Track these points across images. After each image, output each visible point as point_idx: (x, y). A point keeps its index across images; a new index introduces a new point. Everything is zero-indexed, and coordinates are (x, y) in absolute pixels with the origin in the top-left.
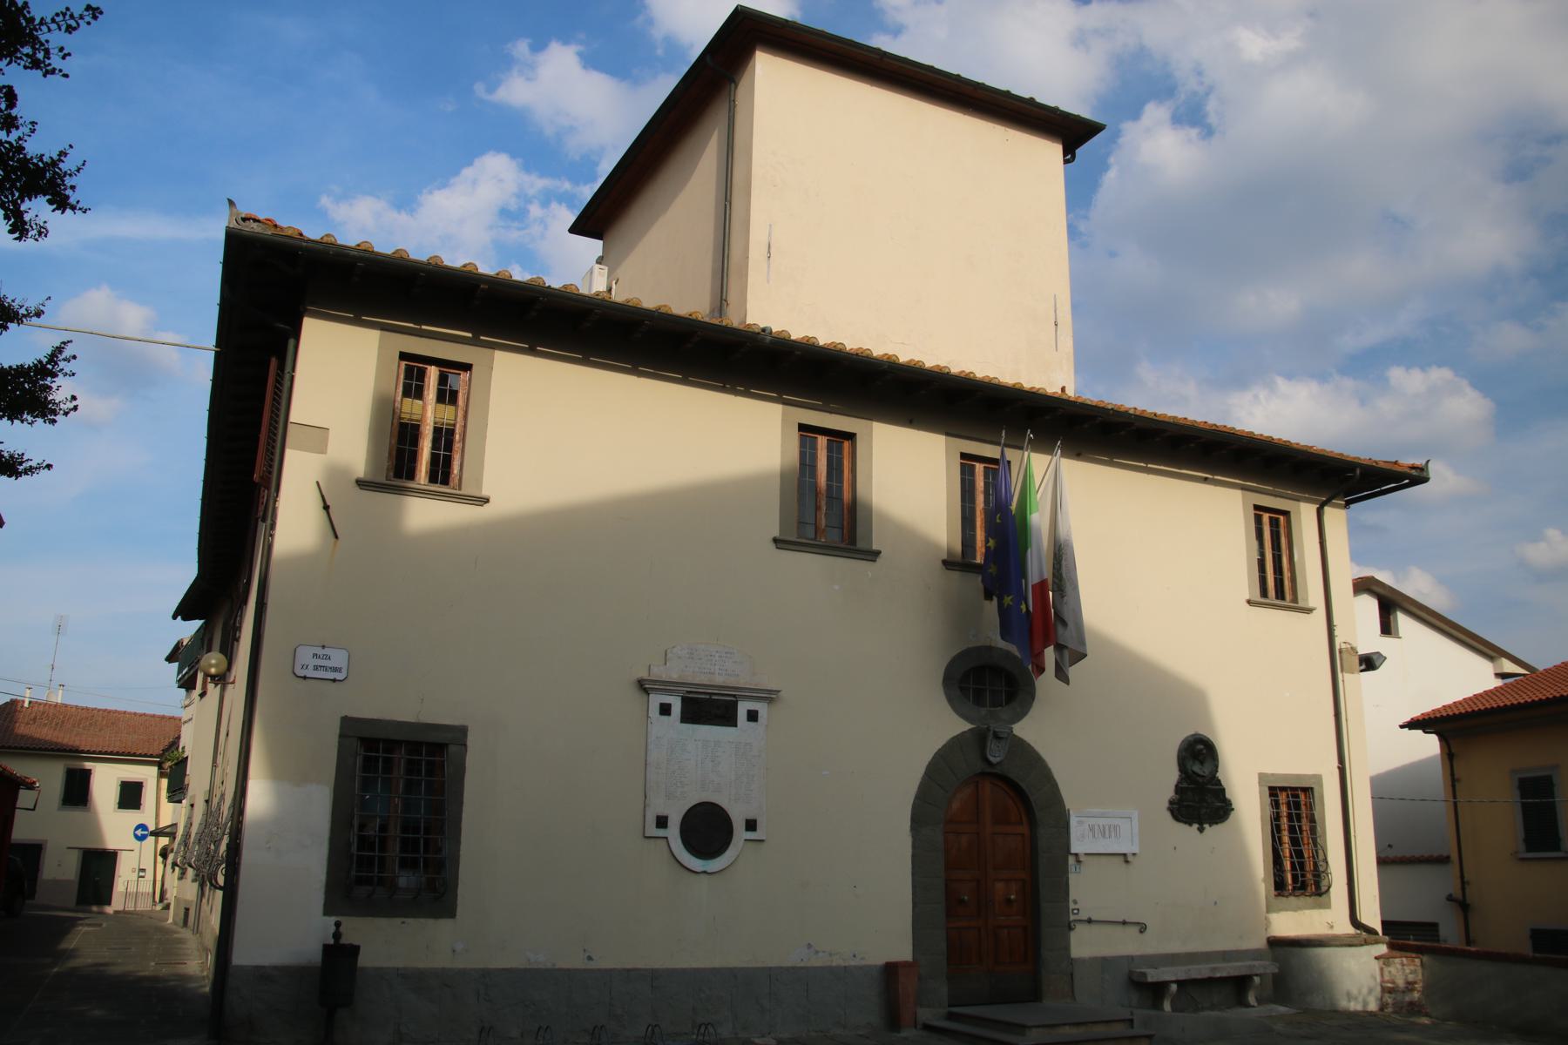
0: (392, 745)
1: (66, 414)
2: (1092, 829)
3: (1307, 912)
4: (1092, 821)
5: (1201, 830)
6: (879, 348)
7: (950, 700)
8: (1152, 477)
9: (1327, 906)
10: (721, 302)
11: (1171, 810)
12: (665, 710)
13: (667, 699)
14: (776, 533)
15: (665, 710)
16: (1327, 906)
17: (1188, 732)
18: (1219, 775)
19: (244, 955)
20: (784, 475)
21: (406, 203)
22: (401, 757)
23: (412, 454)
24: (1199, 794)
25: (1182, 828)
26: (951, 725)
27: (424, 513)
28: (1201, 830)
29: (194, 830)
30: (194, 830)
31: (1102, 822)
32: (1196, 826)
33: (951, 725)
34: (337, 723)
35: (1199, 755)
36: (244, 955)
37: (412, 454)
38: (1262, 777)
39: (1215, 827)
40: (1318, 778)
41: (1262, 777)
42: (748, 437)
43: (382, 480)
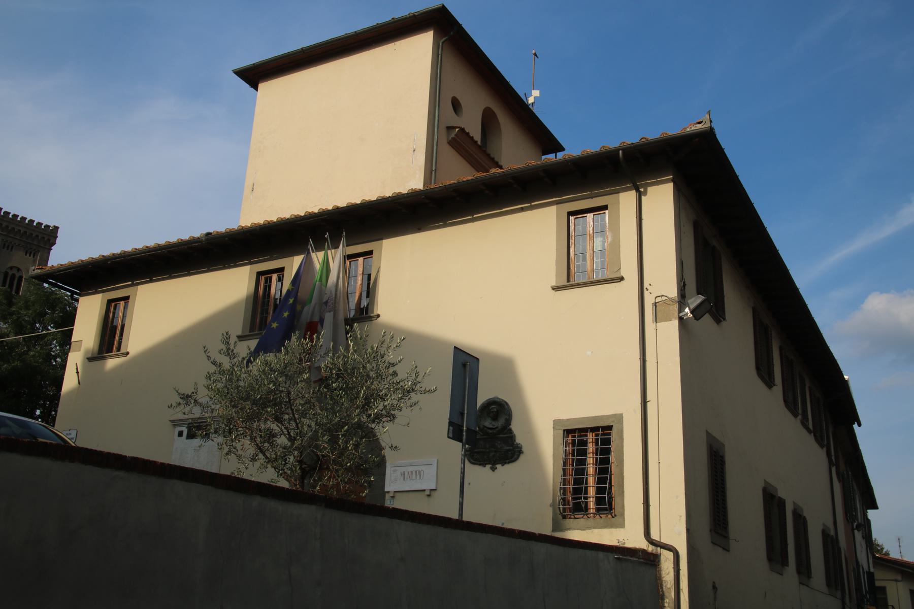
0: (583, 431)
1: (220, 365)
2: (403, 475)
3: (596, 531)
5: (493, 469)
8: (535, 211)
9: (622, 525)
12: (180, 434)
14: (554, 284)
15: (180, 434)
16: (622, 525)
18: (515, 427)
20: (248, 298)
23: (110, 336)
27: (112, 363)
28: (493, 469)
31: (410, 469)
32: (488, 467)
34: (52, 224)
37: (110, 336)
38: (556, 423)
39: (506, 466)
40: (619, 418)
41: (556, 423)
42: (231, 286)
43: (248, 333)
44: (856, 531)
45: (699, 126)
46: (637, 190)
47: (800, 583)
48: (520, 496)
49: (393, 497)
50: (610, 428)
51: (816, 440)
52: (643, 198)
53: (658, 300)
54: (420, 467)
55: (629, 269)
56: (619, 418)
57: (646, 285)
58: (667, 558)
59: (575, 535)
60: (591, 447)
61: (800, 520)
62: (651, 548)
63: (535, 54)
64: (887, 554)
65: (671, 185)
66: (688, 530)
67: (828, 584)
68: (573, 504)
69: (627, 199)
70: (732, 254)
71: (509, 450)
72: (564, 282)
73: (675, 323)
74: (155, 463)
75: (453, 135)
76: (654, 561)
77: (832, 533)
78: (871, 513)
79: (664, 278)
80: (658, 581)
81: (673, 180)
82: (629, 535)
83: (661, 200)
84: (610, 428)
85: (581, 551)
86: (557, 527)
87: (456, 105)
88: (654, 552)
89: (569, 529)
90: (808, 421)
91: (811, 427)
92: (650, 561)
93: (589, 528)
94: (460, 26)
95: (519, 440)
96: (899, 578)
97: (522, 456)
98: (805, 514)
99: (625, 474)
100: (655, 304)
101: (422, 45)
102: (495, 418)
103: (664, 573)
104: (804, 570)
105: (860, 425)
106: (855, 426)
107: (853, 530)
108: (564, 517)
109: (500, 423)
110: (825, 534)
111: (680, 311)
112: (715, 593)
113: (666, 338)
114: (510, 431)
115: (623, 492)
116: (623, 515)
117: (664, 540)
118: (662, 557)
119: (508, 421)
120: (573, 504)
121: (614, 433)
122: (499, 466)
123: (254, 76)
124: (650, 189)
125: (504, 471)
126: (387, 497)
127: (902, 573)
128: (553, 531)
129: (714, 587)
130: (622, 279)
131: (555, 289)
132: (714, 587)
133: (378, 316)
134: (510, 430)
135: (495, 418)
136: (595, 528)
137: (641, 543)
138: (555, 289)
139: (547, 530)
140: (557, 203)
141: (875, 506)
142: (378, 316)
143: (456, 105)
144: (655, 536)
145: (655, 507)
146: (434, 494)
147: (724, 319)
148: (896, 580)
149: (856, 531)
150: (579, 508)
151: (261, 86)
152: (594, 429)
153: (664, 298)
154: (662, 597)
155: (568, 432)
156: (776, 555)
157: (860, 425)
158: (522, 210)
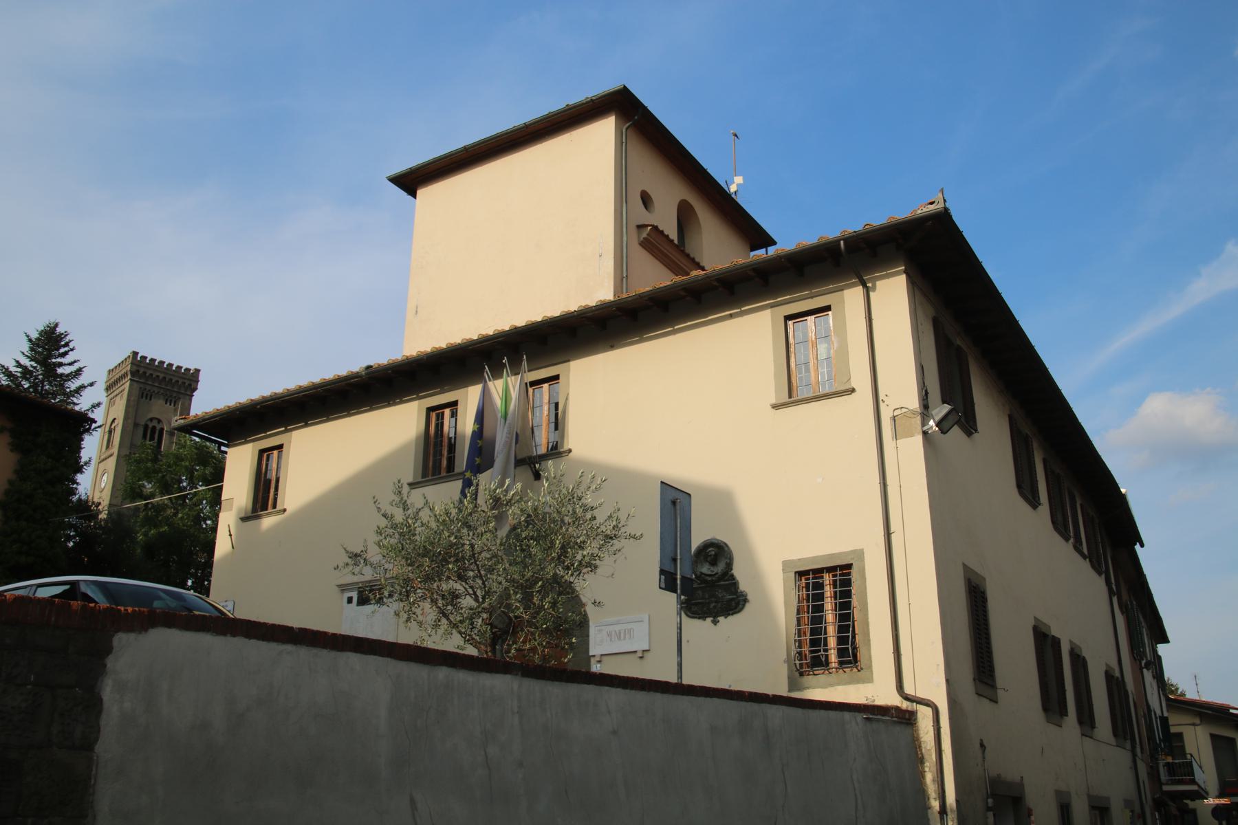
0: (818, 572)
2: (609, 635)
3: (840, 688)
4: (611, 628)
5: (715, 622)
6: (316, 378)
8: (746, 317)
9: (870, 680)
11: (746, 601)
12: (350, 600)
13: (350, 594)
14: (774, 401)
16: (870, 680)
17: (721, 537)
18: (737, 571)
20: (417, 438)
21: (81, 423)
22: (827, 578)
23: (265, 493)
28: (715, 622)
31: (617, 628)
32: (709, 620)
36: (859, 291)
37: (265, 493)
38: (786, 565)
39: (730, 618)
40: (860, 554)
41: (786, 565)
42: (397, 426)
46: (864, 285)
48: (749, 650)
50: (849, 566)
51: (1093, 567)
56: (860, 554)
57: (881, 397)
60: (828, 591)
62: (905, 705)
64: (1183, 694)
66: (947, 681)
67: (1115, 734)
68: (811, 658)
69: (852, 297)
71: (732, 600)
72: (786, 399)
73: (919, 439)
75: (644, 235)
77: (1117, 674)
78: (1162, 649)
80: (915, 743)
81: (905, 272)
83: (893, 294)
84: (849, 566)
86: (793, 685)
87: (646, 199)
91: (1085, 551)
93: (832, 685)
94: (645, 108)
95: (743, 586)
96: (1198, 721)
97: (747, 605)
100: (894, 418)
101: (605, 130)
102: (714, 563)
104: (1087, 720)
105: (1142, 545)
106: (1137, 547)
107: (1141, 669)
108: (801, 674)
109: (720, 568)
110: (1109, 676)
113: (909, 455)
116: (870, 667)
117: (920, 695)
119: (729, 566)
120: (811, 658)
122: (721, 619)
123: (411, 182)
126: (593, 660)
129: (982, 745)
130: (853, 390)
131: (776, 407)
132: (982, 745)
133: (570, 451)
134: (732, 575)
135: (714, 563)
136: (839, 684)
138: (776, 407)
139: (782, 690)
140: (772, 306)
141: (1165, 640)
142: (570, 451)
143: (646, 199)
145: (908, 656)
148: (1194, 724)
150: (818, 662)
151: (420, 192)
152: (830, 570)
154: (922, 761)
155: (800, 574)
157: (1142, 545)
158: (731, 316)
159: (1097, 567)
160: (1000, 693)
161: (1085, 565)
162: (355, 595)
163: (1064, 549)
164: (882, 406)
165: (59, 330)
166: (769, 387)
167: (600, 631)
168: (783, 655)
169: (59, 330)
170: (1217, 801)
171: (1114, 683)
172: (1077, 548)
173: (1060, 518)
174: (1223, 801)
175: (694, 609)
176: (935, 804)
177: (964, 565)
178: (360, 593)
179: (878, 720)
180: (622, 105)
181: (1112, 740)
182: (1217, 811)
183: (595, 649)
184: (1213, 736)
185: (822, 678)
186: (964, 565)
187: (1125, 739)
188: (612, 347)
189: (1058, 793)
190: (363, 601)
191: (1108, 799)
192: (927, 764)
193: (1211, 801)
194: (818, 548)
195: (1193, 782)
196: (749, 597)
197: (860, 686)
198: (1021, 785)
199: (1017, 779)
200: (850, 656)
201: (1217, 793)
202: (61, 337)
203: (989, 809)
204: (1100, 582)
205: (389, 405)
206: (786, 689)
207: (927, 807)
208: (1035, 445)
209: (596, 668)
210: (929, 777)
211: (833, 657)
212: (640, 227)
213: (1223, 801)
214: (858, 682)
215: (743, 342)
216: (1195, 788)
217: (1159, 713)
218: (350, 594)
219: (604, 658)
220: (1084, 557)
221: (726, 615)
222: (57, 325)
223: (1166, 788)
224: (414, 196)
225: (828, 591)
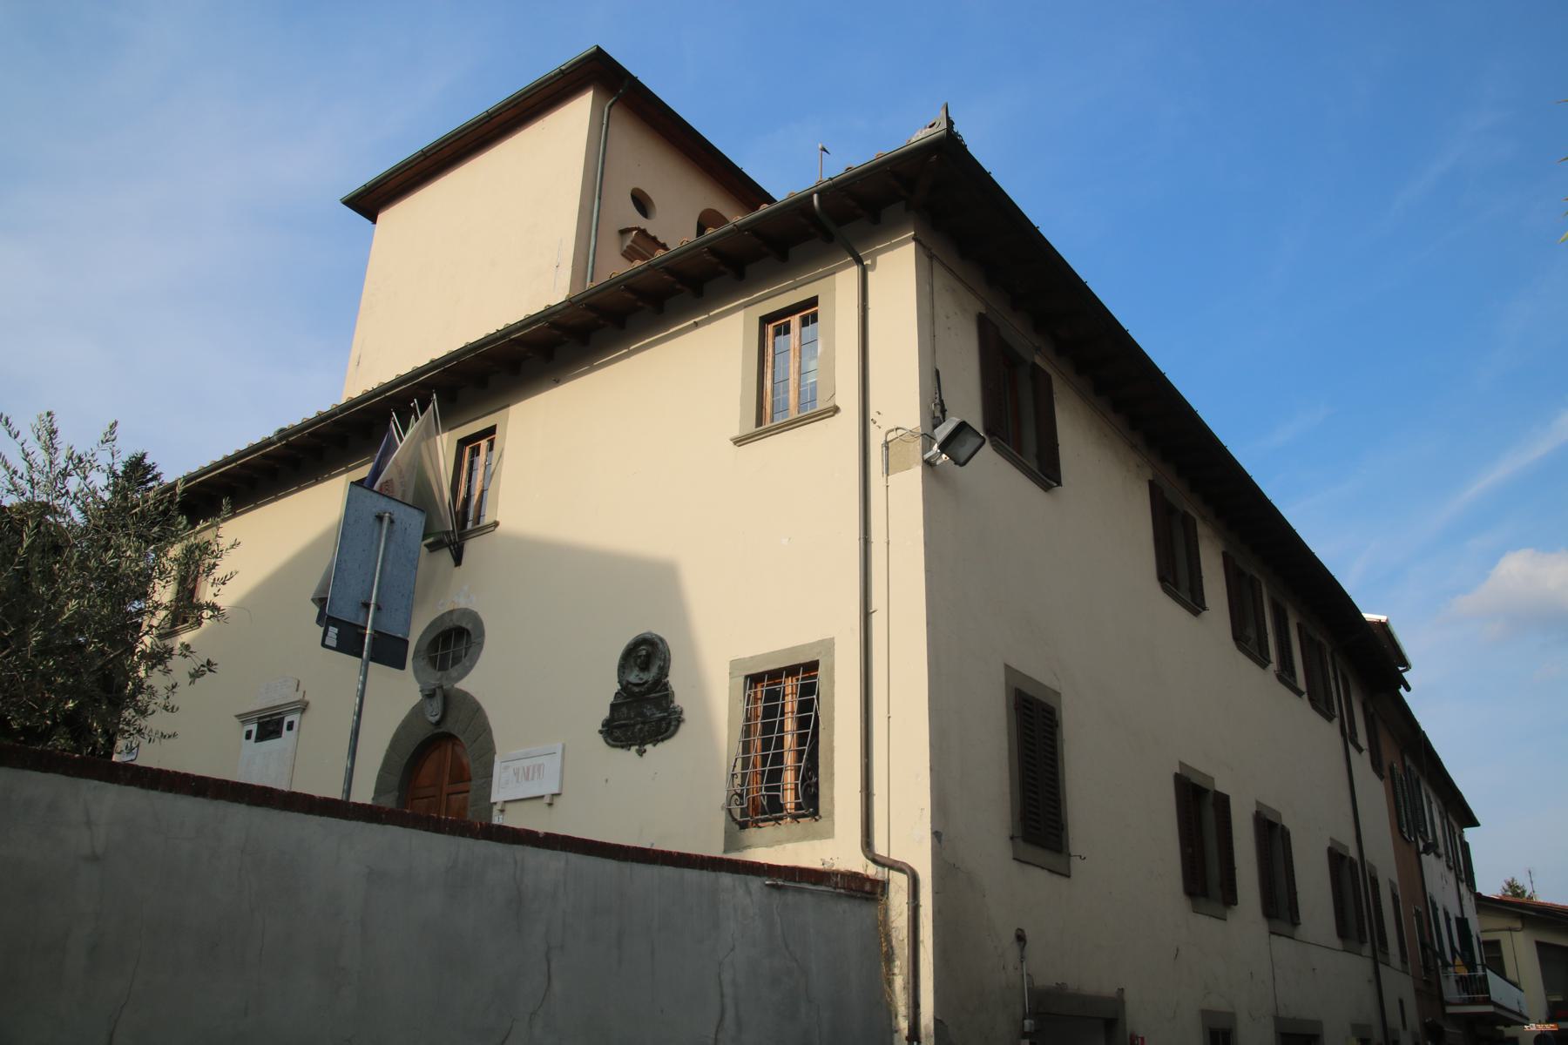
0: (775, 675)
2: (516, 774)
3: (789, 846)
4: (517, 764)
5: (641, 753)
7: (480, 645)
9: (829, 834)
10: (348, 791)
13: (248, 727)
14: (736, 433)
16: (829, 834)
18: (675, 680)
19: (854, 271)
24: (643, 706)
25: (619, 753)
26: (472, 683)
28: (641, 753)
29: (1457, 945)
30: (1457, 945)
31: (526, 763)
32: (634, 748)
33: (472, 683)
35: (646, 657)
36: (854, 271)
38: (734, 664)
39: (660, 745)
40: (828, 645)
41: (734, 664)
44: (1424, 856)
45: (934, 129)
46: (859, 261)
47: (1272, 933)
48: (678, 795)
49: (502, 811)
50: (812, 666)
51: (1315, 707)
52: (870, 274)
53: (891, 436)
54: (549, 763)
55: (847, 398)
56: (828, 645)
57: (872, 414)
58: (899, 882)
59: (761, 854)
60: (785, 699)
61: (1270, 832)
62: (872, 871)
63: (824, 150)
64: (1530, 898)
65: (912, 245)
66: (936, 835)
67: (1342, 932)
68: (757, 806)
69: (846, 280)
70: (1047, 362)
71: (663, 718)
72: (751, 427)
73: (917, 471)
74: (311, 797)
75: (628, 242)
76: (873, 893)
77: (1353, 853)
78: (1469, 834)
79: (900, 402)
80: (882, 929)
81: (915, 239)
82: (835, 849)
83: (897, 269)
84: (812, 666)
85: (669, 871)
86: (731, 842)
87: (642, 203)
88: (879, 877)
89: (749, 847)
90: (1293, 674)
91: (1301, 683)
92: (864, 891)
93: (780, 842)
94: (634, 80)
95: (680, 700)
96: (1518, 925)
97: (683, 727)
98: (1287, 821)
99: (836, 744)
100: (886, 445)
101: (578, 113)
102: (645, 667)
103: (893, 914)
104: (1280, 906)
105: (1408, 689)
106: (1402, 690)
107: (1418, 854)
108: (743, 826)
109: (650, 676)
110: (1336, 858)
111: (924, 452)
112: (1022, 949)
113: (903, 495)
114: (666, 686)
115: (832, 774)
116: (831, 814)
117: (896, 856)
118: (892, 886)
119: (664, 671)
120: (757, 806)
121: (821, 672)
122: (649, 747)
123: (370, 201)
124: (880, 259)
125: (656, 752)
126: (496, 809)
127: (1522, 917)
128: (725, 851)
129: (1021, 938)
130: (836, 410)
131: (739, 441)
132: (1021, 938)
133: (496, 524)
134: (666, 684)
135: (645, 667)
136: (788, 841)
137: (856, 863)
138: (739, 441)
139: (716, 850)
140: (746, 305)
141: (1474, 823)
142: (496, 524)
143: (642, 203)
144: (880, 849)
145: (888, 802)
146: (557, 800)
147: (1059, 484)
148: (1510, 930)
149: (1424, 856)
150: (773, 810)
151: (381, 217)
152: (792, 671)
153: (900, 432)
154: (889, 958)
155: (754, 679)
156: (1206, 880)
157: (1408, 689)
158: (696, 325)
159: (1322, 704)
160: (1076, 864)
161: (1301, 708)
162: (254, 728)
163: (1264, 681)
164: (872, 428)
165: (148, 461)
166: (734, 412)
167: (506, 768)
168: (721, 797)
169: (148, 461)
170: (1541, 1027)
171: (1345, 869)
172: (1286, 675)
173: (1251, 633)
174: (1549, 1027)
175: (617, 733)
176: (903, 1024)
177: (1007, 667)
178: (260, 726)
179: (801, 891)
180: (595, 72)
181: (1336, 943)
182: (1541, 1039)
183: (497, 796)
184: (1538, 944)
185: (769, 830)
186: (1007, 667)
187: (1362, 942)
188: (557, 382)
189: (1206, 1014)
190: (262, 737)
191: (1319, 1024)
192: (898, 963)
193: (1533, 1027)
194: (774, 641)
195: (1488, 1001)
196: (685, 716)
197: (816, 843)
198: (1119, 1001)
199: (1109, 990)
200: (811, 803)
201: (1544, 1017)
202: (148, 469)
203: (1025, 1035)
204: (1330, 732)
205: (317, 482)
206: (722, 847)
207: (892, 1030)
208: (1203, 530)
209: (497, 820)
210: (899, 982)
211: (789, 799)
212: (624, 232)
213: (1549, 1027)
214: (814, 838)
215: (709, 355)
216: (1490, 1009)
217: (1454, 912)
218: (248, 727)
219: (508, 806)
220: (1299, 693)
221: (655, 742)
222: (144, 456)
223: (1450, 1010)
224: (374, 221)
225: (785, 699)
